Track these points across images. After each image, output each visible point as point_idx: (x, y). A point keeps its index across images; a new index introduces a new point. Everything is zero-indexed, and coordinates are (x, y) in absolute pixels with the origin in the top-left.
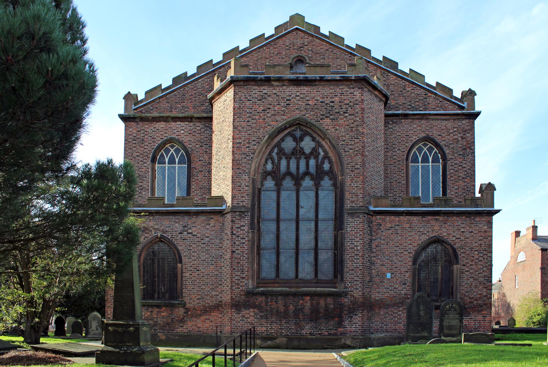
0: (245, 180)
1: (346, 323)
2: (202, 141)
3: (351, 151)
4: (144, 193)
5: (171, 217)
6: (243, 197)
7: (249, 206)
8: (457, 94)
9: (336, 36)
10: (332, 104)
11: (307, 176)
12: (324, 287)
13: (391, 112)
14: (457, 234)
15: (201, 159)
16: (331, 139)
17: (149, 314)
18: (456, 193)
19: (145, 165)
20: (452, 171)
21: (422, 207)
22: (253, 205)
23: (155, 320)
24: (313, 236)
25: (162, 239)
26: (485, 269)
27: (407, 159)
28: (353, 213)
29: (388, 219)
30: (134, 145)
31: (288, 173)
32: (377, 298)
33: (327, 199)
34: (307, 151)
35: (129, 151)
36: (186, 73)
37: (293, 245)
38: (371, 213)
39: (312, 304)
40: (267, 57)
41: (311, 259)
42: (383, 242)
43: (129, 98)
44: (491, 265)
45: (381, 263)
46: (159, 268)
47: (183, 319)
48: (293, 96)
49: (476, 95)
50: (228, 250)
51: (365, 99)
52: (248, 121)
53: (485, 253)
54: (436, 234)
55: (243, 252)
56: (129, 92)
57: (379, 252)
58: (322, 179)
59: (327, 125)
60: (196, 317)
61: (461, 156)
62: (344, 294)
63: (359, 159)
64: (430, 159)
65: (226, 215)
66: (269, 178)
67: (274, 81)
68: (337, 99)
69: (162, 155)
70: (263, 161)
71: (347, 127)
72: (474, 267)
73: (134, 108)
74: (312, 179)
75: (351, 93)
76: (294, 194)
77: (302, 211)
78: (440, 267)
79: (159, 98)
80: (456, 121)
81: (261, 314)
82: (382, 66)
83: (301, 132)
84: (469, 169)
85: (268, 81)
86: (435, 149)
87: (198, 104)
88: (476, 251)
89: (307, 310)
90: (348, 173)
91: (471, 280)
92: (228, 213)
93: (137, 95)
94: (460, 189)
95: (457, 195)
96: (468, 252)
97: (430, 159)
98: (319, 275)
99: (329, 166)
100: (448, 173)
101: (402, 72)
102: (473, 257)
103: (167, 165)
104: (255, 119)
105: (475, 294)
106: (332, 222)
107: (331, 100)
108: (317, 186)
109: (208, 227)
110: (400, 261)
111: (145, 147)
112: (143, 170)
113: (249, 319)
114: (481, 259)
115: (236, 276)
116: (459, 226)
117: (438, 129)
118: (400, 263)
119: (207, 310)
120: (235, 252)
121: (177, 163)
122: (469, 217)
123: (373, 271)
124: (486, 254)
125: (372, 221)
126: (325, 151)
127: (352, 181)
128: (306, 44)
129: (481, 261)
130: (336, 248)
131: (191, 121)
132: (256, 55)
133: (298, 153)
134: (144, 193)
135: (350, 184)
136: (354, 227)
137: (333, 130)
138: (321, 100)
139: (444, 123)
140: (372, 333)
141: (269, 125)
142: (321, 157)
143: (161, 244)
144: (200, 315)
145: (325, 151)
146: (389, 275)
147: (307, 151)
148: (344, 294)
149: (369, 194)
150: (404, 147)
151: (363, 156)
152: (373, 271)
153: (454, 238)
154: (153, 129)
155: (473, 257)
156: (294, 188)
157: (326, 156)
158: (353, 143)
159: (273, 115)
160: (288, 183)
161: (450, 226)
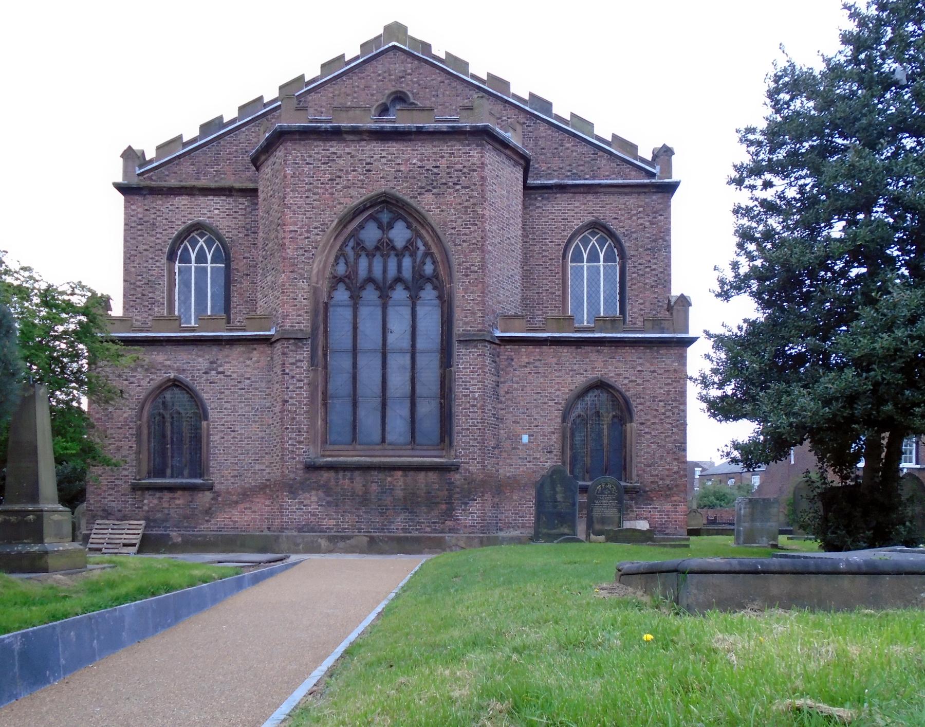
0: (303, 289)
1: (458, 513)
2: (248, 227)
3: (465, 244)
4: (156, 309)
5: (191, 347)
6: (299, 316)
7: (309, 330)
8: (646, 152)
9: (456, 59)
10: (436, 170)
11: (399, 284)
12: (424, 457)
13: (539, 182)
14: (632, 375)
15: (246, 255)
16: (434, 225)
17: (156, 501)
18: (641, 310)
19: (158, 264)
20: (634, 275)
21: (576, 331)
22: (314, 329)
23: (166, 511)
24: (408, 375)
25: (176, 384)
26: (675, 430)
27: (564, 257)
28: (467, 342)
29: (523, 350)
30: (139, 233)
31: (370, 280)
32: (508, 474)
33: (429, 320)
34: (399, 243)
35: (133, 242)
36: (221, 118)
37: (378, 390)
38: (497, 341)
39: (405, 484)
40: (349, 92)
41: (405, 412)
42: (515, 386)
43: (130, 155)
44: (685, 424)
45: (513, 419)
46: (172, 428)
47: (210, 509)
48: (376, 157)
49: (673, 153)
50: (278, 400)
51: (487, 161)
52: (307, 197)
53: (675, 404)
54: (599, 375)
55: (300, 402)
56: (130, 147)
57: (510, 402)
58: (421, 288)
59: (428, 204)
60: (230, 505)
61: (649, 252)
62: (455, 468)
63: (476, 257)
64: (602, 256)
65: (275, 345)
66: (341, 287)
67: (347, 133)
68: (443, 163)
69: (186, 249)
70: (332, 259)
71: (459, 207)
72: (658, 426)
73: (138, 172)
74: (407, 288)
75: (466, 153)
76: (379, 312)
77: (391, 338)
78: (605, 427)
79: (179, 157)
80: (642, 197)
81: (329, 499)
82: (527, 108)
83: (391, 215)
84: (661, 272)
85: (336, 134)
86: (610, 241)
87: (241, 168)
88: (660, 401)
89: (399, 493)
90: (459, 279)
91: (654, 446)
92: (278, 340)
93: (143, 153)
94: (647, 304)
95: (642, 312)
96: (648, 403)
97: (602, 256)
98: (417, 438)
99: (432, 267)
100: (628, 278)
101: (558, 118)
102: (657, 410)
103: (209, 266)
104: (318, 194)
105: (660, 469)
106: (434, 354)
107: (434, 164)
108: (414, 300)
109: (248, 362)
110: (542, 416)
111: (158, 236)
112: (154, 273)
113: (308, 507)
114: (668, 413)
115: (290, 439)
116: (634, 361)
117: (609, 210)
118: (542, 419)
119: (246, 495)
120: (287, 401)
121: (209, 261)
122: (651, 348)
123: (502, 432)
124: (676, 407)
125: (499, 353)
126: (426, 244)
127: (466, 290)
128: (409, 71)
129: (669, 417)
130: (443, 396)
131: (230, 196)
132: (331, 90)
133: (385, 248)
134: (156, 309)
135: (463, 296)
136: (469, 364)
137: (437, 211)
138: (419, 164)
139: (623, 199)
140: (501, 530)
141: (340, 203)
142: (420, 253)
143: (176, 390)
144: (237, 503)
145: (426, 244)
146: (525, 439)
147: (399, 243)
148: (455, 468)
149: (494, 312)
150: (559, 236)
151: (483, 251)
152: (502, 432)
153: (626, 381)
154: (171, 208)
155: (657, 410)
156: (379, 302)
157: (428, 254)
158: (467, 231)
159: (345, 187)
160: (370, 294)
161: (619, 361)
